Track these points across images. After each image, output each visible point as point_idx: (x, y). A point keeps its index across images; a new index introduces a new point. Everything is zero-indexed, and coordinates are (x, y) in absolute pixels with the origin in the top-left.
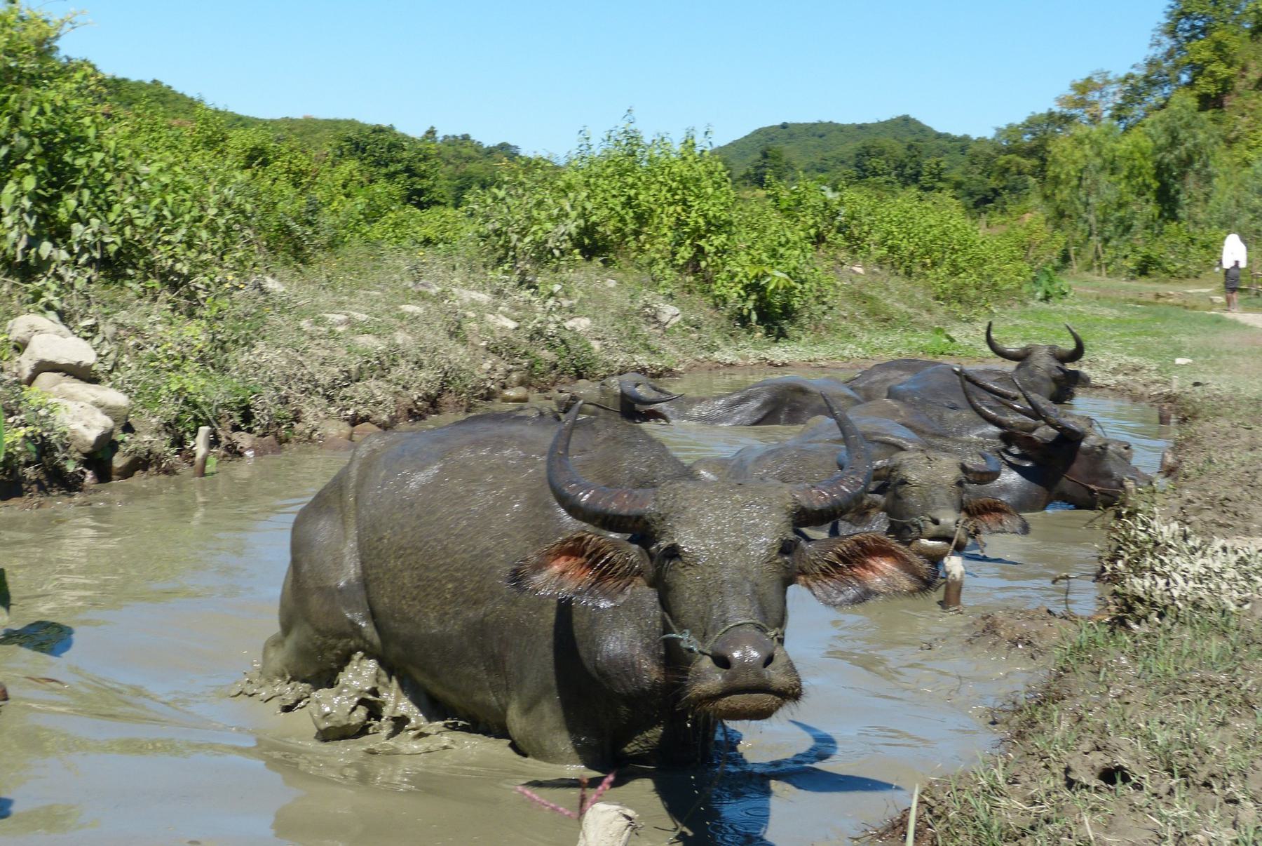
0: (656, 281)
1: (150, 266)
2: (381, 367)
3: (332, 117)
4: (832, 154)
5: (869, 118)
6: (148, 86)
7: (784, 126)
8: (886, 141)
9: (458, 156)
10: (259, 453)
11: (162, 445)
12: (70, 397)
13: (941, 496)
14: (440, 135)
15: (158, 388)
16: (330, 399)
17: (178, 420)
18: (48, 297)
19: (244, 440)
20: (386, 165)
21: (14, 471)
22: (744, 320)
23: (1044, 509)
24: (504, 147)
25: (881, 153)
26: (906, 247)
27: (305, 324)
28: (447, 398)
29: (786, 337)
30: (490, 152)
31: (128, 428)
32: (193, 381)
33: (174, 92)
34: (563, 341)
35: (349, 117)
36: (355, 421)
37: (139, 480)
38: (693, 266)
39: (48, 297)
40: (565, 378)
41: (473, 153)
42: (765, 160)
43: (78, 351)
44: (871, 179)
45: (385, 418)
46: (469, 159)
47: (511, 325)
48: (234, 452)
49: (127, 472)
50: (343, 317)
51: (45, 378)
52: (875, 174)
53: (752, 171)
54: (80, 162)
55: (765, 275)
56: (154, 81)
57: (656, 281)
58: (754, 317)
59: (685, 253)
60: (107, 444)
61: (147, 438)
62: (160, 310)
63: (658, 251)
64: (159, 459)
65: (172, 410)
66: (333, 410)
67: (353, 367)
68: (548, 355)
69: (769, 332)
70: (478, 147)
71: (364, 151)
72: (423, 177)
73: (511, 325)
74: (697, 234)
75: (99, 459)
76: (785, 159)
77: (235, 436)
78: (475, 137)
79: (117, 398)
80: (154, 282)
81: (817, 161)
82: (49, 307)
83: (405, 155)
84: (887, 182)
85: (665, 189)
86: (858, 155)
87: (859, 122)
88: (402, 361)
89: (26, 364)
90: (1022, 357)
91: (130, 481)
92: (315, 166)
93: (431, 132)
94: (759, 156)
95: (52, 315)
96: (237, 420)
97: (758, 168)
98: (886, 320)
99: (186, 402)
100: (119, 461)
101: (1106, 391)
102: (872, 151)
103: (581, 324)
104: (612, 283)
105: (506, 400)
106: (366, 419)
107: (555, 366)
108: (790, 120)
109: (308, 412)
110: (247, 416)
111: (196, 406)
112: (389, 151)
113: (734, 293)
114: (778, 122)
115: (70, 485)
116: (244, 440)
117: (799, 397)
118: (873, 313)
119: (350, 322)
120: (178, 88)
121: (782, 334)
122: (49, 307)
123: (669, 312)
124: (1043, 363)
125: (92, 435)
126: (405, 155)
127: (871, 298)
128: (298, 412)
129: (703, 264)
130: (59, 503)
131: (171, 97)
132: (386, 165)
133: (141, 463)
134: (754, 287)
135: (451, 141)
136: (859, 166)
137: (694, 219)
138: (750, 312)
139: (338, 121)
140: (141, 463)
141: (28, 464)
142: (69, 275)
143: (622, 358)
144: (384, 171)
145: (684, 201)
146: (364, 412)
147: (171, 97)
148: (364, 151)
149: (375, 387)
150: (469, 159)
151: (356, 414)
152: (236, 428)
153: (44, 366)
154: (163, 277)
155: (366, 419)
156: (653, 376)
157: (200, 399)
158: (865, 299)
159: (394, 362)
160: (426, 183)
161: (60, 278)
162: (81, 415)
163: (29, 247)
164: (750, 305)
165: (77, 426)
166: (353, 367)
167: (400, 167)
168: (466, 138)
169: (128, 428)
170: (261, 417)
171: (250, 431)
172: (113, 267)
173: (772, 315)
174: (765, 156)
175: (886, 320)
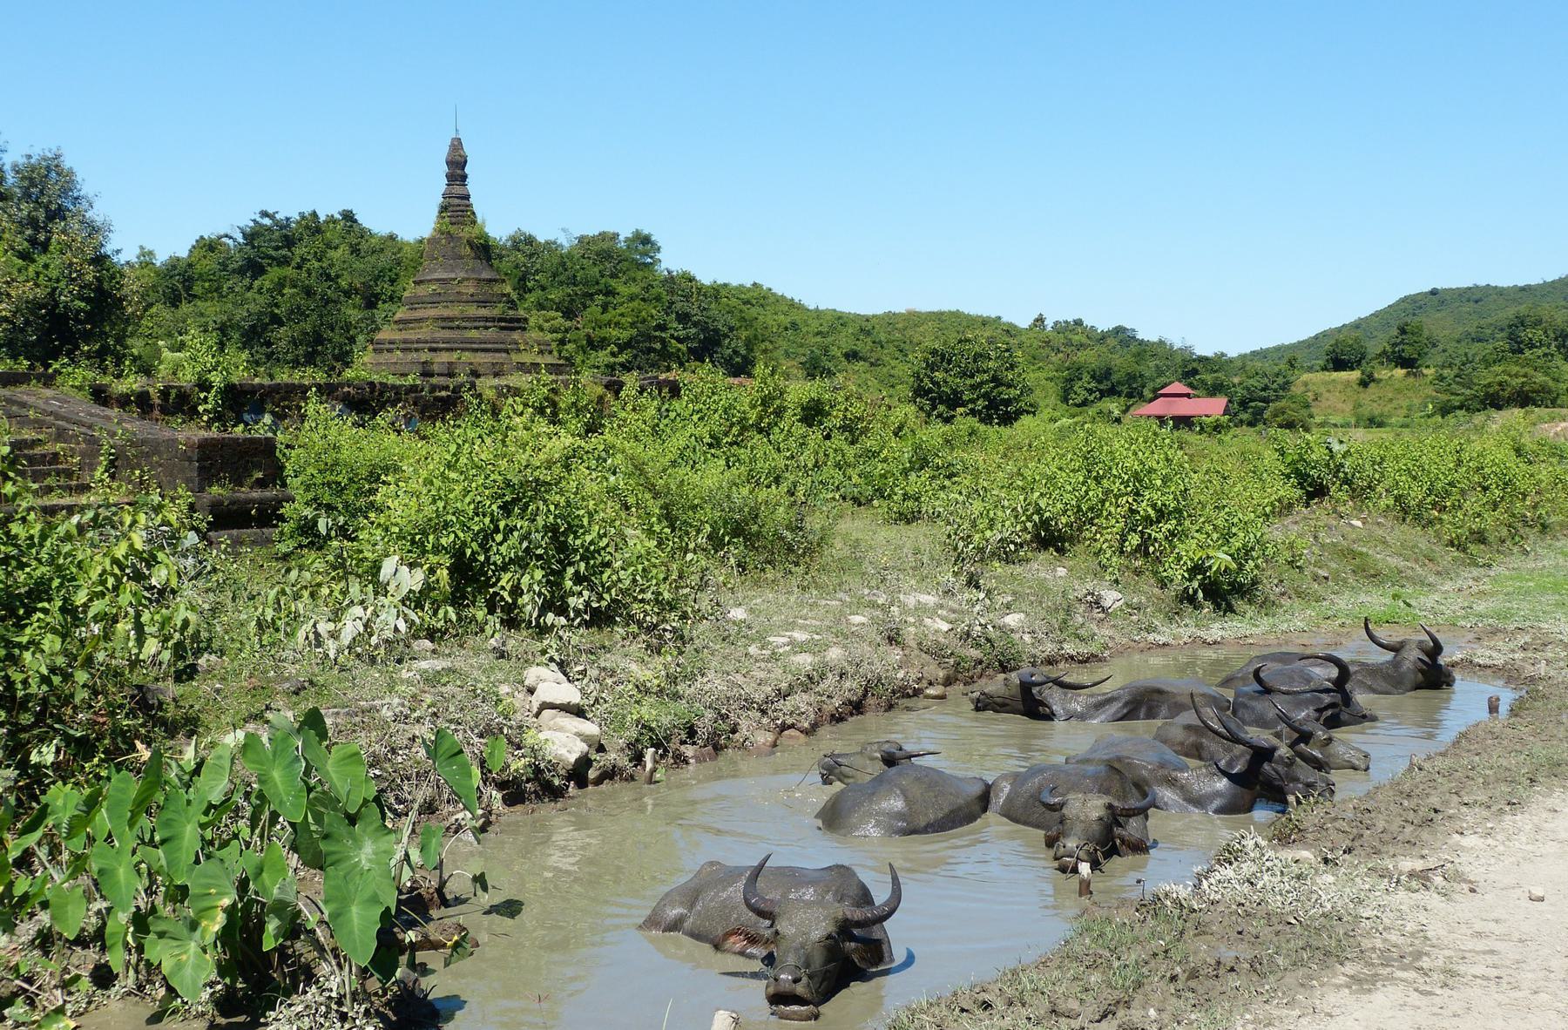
0: (1104, 568)
1: (631, 617)
2: (810, 681)
3: (935, 309)
4: (1489, 320)
5: (1534, 279)
6: (749, 290)
7: (1434, 292)
8: (1545, 310)
9: (1069, 343)
10: (699, 760)
11: (624, 761)
12: (560, 729)
13: (1078, 828)
14: (1049, 323)
15: (624, 717)
16: (764, 712)
17: (637, 740)
18: (552, 652)
19: (689, 751)
20: (972, 376)
21: (519, 786)
22: (1192, 599)
23: (1250, 810)
24: (1119, 330)
25: (1538, 323)
26: (1416, 494)
27: (753, 650)
28: (870, 701)
29: (1233, 611)
30: (1103, 337)
31: (601, 749)
32: (648, 711)
33: (774, 295)
34: (988, 640)
35: (953, 309)
36: (784, 727)
37: (606, 786)
38: (1142, 550)
39: (552, 652)
40: (990, 672)
41: (1084, 340)
42: (1392, 347)
43: (569, 693)
44: (1528, 353)
45: (806, 725)
46: (1081, 346)
47: (945, 627)
48: (680, 760)
49: (598, 781)
50: (786, 640)
51: (547, 713)
52: (1532, 346)
53: (1388, 348)
54: (578, 542)
55: (1208, 557)
56: (755, 284)
57: (1104, 568)
58: (1200, 594)
59: (1134, 540)
60: (584, 762)
61: (613, 756)
62: (636, 647)
63: (1106, 541)
64: (621, 770)
65: (633, 733)
66: (765, 720)
67: (784, 686)
68: (975, 653)
69: (1218, 606)
70: (1090, 332)
71: (949, 362)
72: (1009, 386)
73: (945, 627)
74: (1148, 521)
75: (579, 773)
76: (1426, 333)
77: (683, 748)
78: (1088, 322)
79: (591, 728)
80: (634, 628)
81: (1472, 330)
82: (552, 659)
83: (991, 364)
84: (1545, 355)
85: (1118, 482)
86: (1510, 326)
87: (1521, 284)
88: (830, 675)
89: (536, 702)
90: (1396, 648)
91: (603, 787)
92: (869, 411)
93: (1040, 320)
94: (1395, 332)
95: (553, 666)
96: (684, 737)
97: (1395, 345)
98: (1374, 576)
99: (644, 726)
100: (592, 774)
101: (1489, 671)
102: (1528, 321)
103: (1012, 620)
104: (1061, 572)
105: (928, 697)
106: (792, 726)
107: (981, 662)
108: (1440, 285)
109: (744, 724)
110: (691, 732)
111: (651, 729)
112: (975, 361)
113: (1178, 574)
114: (1427, 289)
115: (556, 793)
116: (689, 751)
117: (1156, 696)
118: (1359, 571)
119: (792, 642)
120: (778, 290)
121: (1230, 609)
122: (552, 659)
123: (1111, 597)
124: (1412, 655)
125: (572, 758)
126: (991, 364)
127: (1361, 554)
128: (736, 724)
129: (1151, 549)
130: (547, 809)
131: (772, 300)
132: (972, 376)
133: (609, 774)
134: (1197, 569)
135: (1063, 328)
136: (1513, 338)
137: (1144, 508)
138: (1195, 592)
139: (942, 313)
140: (609, 774)
141: (528, 781)
142: (566, 635)
143: (1049, 648)
144: (969, 382)
145: (1137, 494)
146: (790, 721)
147: (772, 300)
148: (949, 362)
149: (800, 700)
150: (1081, 346)
151: (784, 723)
152: (683, 742)
153: (545, 706)
154: (640, 623)
155: (792, 726)
156: (1080, 662)
157: (654, 725)
158: (1354, 554)
159: (822, 677)
160: (1014, 393)
161: (561, 638)
162: (563, 742)
163: (539, 616)
164: (1196, 584)
165: (563, 751)
166: (784, 686)
167: (986, 377)
168: (1078, 323)
169: (601, 749)
170: (703, 730)
171: (694, 743)
172: (599, 619)
173: (1221, 593)
174: (1403, 331)
175: (1374, 576)
